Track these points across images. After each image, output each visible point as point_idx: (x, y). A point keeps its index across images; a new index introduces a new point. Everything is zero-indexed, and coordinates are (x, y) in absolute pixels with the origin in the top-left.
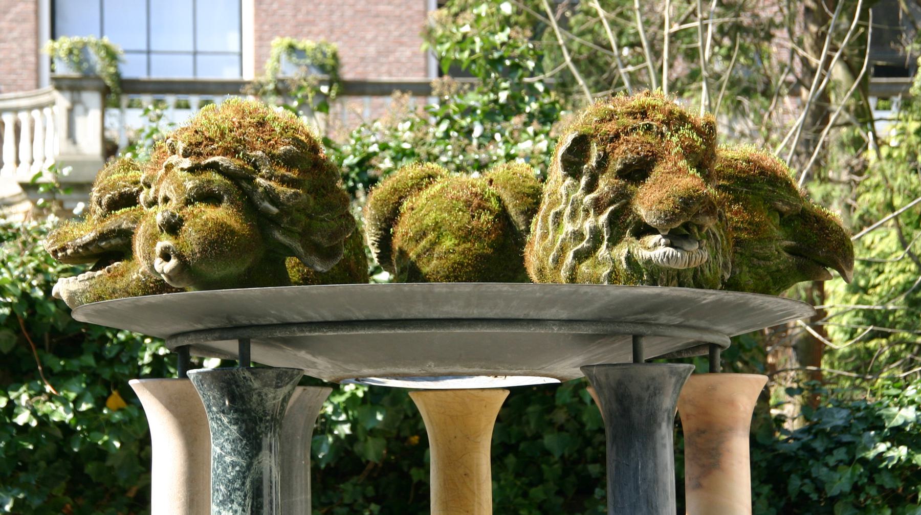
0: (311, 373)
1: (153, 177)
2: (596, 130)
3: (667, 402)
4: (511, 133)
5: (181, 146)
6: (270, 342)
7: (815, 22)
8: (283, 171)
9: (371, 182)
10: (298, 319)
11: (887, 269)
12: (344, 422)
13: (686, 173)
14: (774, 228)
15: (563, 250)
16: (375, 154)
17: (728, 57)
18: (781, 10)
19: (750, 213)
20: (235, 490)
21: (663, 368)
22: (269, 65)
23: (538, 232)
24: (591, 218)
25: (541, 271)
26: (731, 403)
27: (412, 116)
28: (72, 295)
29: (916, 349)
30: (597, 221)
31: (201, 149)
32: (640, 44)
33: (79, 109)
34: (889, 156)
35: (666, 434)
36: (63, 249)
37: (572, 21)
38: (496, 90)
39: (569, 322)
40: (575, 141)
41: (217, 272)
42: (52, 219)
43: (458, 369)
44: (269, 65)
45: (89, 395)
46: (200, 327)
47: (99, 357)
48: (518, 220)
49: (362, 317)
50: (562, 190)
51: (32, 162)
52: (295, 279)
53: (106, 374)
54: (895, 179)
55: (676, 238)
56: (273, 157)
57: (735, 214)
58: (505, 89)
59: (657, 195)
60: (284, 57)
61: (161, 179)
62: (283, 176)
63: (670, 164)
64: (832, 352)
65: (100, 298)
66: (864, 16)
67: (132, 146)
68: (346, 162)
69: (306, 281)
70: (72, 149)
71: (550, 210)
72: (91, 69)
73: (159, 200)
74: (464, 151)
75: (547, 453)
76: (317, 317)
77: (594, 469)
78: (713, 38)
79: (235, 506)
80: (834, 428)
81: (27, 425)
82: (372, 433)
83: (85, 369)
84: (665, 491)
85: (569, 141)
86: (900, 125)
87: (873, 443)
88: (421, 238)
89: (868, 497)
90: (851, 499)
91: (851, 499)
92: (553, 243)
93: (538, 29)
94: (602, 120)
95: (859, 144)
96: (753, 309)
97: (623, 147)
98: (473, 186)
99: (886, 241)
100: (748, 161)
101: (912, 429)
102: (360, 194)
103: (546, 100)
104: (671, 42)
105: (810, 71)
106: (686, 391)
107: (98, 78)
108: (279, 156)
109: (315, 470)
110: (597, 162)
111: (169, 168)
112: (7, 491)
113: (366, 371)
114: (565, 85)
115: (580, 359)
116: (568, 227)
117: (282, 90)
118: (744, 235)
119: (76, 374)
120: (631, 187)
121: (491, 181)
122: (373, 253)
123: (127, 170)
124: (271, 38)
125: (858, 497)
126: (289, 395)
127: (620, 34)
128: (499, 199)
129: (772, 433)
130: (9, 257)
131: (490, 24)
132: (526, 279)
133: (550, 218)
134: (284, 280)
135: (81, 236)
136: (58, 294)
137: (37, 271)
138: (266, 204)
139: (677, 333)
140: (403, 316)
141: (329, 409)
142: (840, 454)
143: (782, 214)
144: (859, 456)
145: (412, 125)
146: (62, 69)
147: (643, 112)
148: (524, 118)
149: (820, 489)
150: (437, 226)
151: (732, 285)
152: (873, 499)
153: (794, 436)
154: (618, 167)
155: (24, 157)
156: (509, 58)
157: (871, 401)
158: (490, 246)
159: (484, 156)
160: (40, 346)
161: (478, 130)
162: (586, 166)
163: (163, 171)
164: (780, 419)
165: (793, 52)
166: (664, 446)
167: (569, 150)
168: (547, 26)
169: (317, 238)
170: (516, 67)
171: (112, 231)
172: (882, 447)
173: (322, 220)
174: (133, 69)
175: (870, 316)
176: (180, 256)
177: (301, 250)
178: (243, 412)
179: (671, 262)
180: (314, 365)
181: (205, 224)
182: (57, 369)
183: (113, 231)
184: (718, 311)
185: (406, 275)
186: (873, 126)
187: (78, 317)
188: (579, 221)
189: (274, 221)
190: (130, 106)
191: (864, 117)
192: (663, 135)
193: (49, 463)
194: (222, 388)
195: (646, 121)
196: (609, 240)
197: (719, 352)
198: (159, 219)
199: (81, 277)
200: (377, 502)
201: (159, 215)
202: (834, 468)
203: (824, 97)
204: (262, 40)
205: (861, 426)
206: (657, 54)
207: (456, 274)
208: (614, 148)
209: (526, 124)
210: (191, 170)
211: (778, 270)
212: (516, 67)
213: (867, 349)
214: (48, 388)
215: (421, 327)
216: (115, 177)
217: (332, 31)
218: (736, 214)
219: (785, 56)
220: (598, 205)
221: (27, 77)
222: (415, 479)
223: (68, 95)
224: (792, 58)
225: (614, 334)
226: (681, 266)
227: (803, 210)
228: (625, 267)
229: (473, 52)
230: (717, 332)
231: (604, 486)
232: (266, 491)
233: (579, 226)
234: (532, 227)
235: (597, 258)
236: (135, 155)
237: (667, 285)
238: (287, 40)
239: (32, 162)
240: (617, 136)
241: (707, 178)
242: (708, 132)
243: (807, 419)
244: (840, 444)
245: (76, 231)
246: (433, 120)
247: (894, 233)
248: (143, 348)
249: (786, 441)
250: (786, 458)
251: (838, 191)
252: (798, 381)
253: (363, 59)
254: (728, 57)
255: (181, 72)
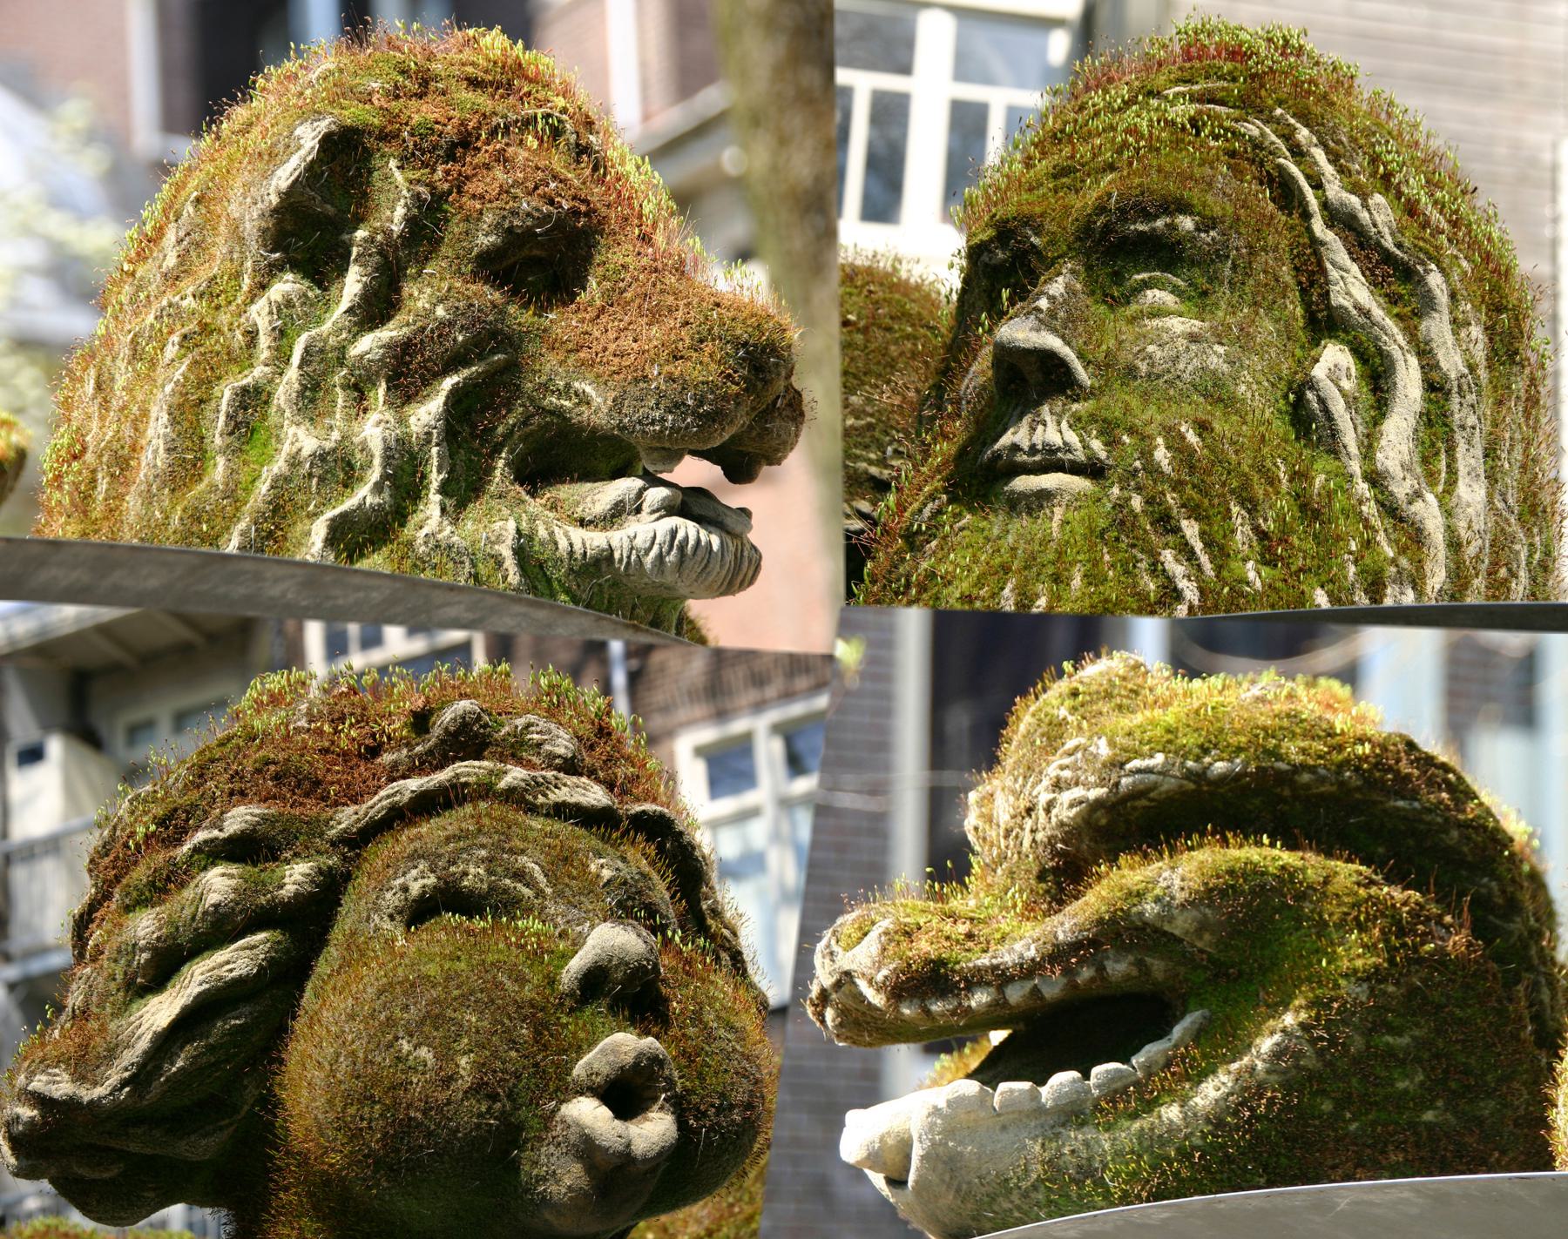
30: (402, 421)
40: (329, 143)
73: (646, 508)
110: (410, 220)
120: (521, 317)
154: (485, 240)
162: (361, 234)
179: (688, 564)
196: (444, 490)
228: (514, 578)
233: (336, 435)
235: (410, 544)
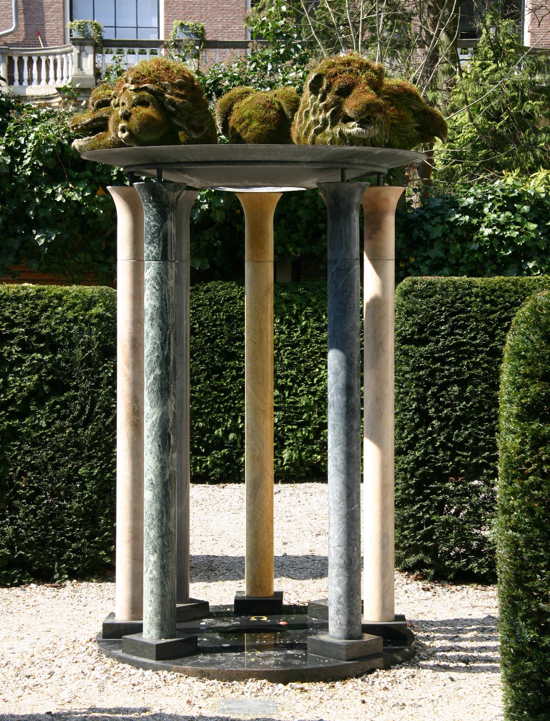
0: (190, 184)
1: (117, 93)
2: (326, 72)
3: (357, 200)
4: (286, 69)
5: (130, 79)
6: (170, 171)
7: (433, 13)
8: (133, 715)
9: (219, 94)
10: (185, 160)
11: (463, 131)
12: (205, 203)
13: (368, 92)
14: (410, 118)
15: (309, 129)
16: (221, 78)
17: (391, 30)
18: (416, 6)
19: (399, 111)
20: (155, 237)
21: (356, 184)
22: (172, 33)
23: (298, 120)
24: (323, 114)
25: (298, 139)
26: (387, 200)
27: (239, 60)
28: (81, 147)
29: (475, 169)
31: (139, 81)
32: (348, 25)
33: (83, 54)
34: (466, 77)
35: (356, 216)
36: (77, 126)
37: (316, 12)
38: (278, 48)
39: (311, 162)
41: (147, 138)
42: (71, 108)
43: (259, 184)
44: (172, 33)
45: (89, 189)
46: (139, 163)
47: (93, 172)
48: (288, 113)
49: (214, 160)
50: (309, 101)
51: (62, 79)
52: (183, 141)
53: (97, 179)
54: (468, 90)
55: (362, 124)
56: (173, 84)
57: (391, 111)
58: (283, 48)
59: (355, 103)
60: (178, 29)
61: (121, 95)
62: (178, 93)
63: (361, 88)
64: (435, 170)
65: (93, 149)
66: (456, 11)
67: (107, 74)
68: (208, 82)
69: (188, 142)
70: (80, 72)
71: (303, 110)
72: (89, 34)
74: (263, 77)
75: (299, 218)
76: (193, 159)
77: (321, 226)
78: (383, 21)
79: (155, 245)
80: (436, 207)
81: (61, 201)
82: (218, 208)
83: (87, 177)
84: (355, 240)
85: (313, 77)
86: (472, 62)
87: (453, 214)
88: (242, 122)
89: (450, 239)
90: (442, 240)
91: (442, 240)
92: (305, 125)
93: (299, 17)
94: (329, 67)
95: (451, 72)
96: (399, 156)
97: (339, 80)
98: (267, 97)
99: (464, 117)
100: (398, 86)
101: (472, 207)
102: (214, 98)
103: (303, 53)
104: (363, 24)
105: (430, 37)
106: (365, 194)
107: (92, 39)
108: (176, 84)
109: (192, 225)
111: (125, 89)
112: (53, 231)
113: (215, 184)
114: (311, 44)
115: (315, 180)
116: (312, 118)
117: (177, 45)
118: (396, 121)
119: (83, 179)
120: (342, 99)
121: (276, 95)
122: (220, 130)
123: (105, 89)
124: (172, 21)
125: (445, 239)
126: (180, 195)
127: (339, 19)
128: (279, 104)
129: (406, 210)
130: (52, 125)
131: (276, 16)
132: (290, 142)
133: (304, 114)
134: (178, 142)
135: (85, 120)
136: (74, 147)
137: (65, 132)
138: (170, 107)
139: (362, 167)
140: (233, 160)
141: (199, 197)
142: (438, 219)
143: (414, 111)
144: (446, 220)
145: (239, 64)
146: (75, 35)
147: (348, 63)
148: (292, 61)
149: (427, 235)
150: (250, 116)
151: (389, 145)
152: (452, 240)
153: (416, 211)
154: (336, 89)
155: (59, 75)
156: (285, 33)
157: (453, 194)
158: (275, 126)
159: (272, 80)
160: (67, 166)
161: (270, 67)
163: (122, 91)
164: (411, 202)
165: (421, 27)
166: (355, 221)
167: (313, 82)
168: (303, 15)
169: (193, 123)
170: (288, 37)
171: (98, 118)
172: (457, 216)
173: (196, 114)
174: (108, 35)
175: (455, 155)
176: (130, 131)
177: (186, 128)
178: (159, 202)
180: (191, 181)
181: (141, 116)
182: (74, 177)
183: (99, 118)
184: (382, 157)
185: (234, 140)
186: (459, 64)
187: (84, 157)
188: (317, 115)
189: (173, 115)
190: (106, 53)
191: (455, 59)
192: (358, 74)
193: (71, 219)
194: (149, 191)
195: (350, 68)
197: (382, 176)
198: (120, 113)
199: (84, 139)
200: (220, 240)
201: (120, 111)
202: (434, 226)
203: (436, 50)
204: (168, 21)
205: (448, 206)
206: (356, 29)
207: (259, 139)
208: (334, 81)
209: (293, 65)
210: (134, 90)
211: (411, 138)
212: (288, 37)
213: (452, 168)
214: (70, 185)
215: (241, 165)
216: (100, 92)
217: (201, 17)
218: (392, 111)
219: (418, 29)
220: (326, 108)
221: (59, 38)
222: (238, 230)
223: (78, 47)
224: (421, 31)
225: (332, 168)
226: (365, 137)
227: (424, 109)
229: (268, 30)
230: (381, 167)
231: (326, 234)
232: (169, 239)
234: (295, 118)
236: (109, 78)
237: (358, 146)
238: (180, 22)
239: (62, 79)
240: (336, 75)
241: (379, 95)
242: (380, 73)
243: (422, 203)
244: (438, 215)
245: (82, 118)
246: (249, 63)
247: (467, 114)
248: (112, 167)
249: (413, 213)
250: (412, 221)
251: (440, 94)
252: (418, 186)
253: (216, 30)
254: (391, 30)
255: (130, 36)
